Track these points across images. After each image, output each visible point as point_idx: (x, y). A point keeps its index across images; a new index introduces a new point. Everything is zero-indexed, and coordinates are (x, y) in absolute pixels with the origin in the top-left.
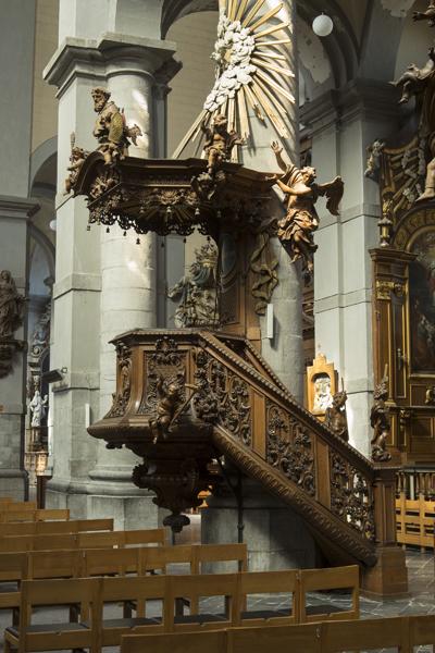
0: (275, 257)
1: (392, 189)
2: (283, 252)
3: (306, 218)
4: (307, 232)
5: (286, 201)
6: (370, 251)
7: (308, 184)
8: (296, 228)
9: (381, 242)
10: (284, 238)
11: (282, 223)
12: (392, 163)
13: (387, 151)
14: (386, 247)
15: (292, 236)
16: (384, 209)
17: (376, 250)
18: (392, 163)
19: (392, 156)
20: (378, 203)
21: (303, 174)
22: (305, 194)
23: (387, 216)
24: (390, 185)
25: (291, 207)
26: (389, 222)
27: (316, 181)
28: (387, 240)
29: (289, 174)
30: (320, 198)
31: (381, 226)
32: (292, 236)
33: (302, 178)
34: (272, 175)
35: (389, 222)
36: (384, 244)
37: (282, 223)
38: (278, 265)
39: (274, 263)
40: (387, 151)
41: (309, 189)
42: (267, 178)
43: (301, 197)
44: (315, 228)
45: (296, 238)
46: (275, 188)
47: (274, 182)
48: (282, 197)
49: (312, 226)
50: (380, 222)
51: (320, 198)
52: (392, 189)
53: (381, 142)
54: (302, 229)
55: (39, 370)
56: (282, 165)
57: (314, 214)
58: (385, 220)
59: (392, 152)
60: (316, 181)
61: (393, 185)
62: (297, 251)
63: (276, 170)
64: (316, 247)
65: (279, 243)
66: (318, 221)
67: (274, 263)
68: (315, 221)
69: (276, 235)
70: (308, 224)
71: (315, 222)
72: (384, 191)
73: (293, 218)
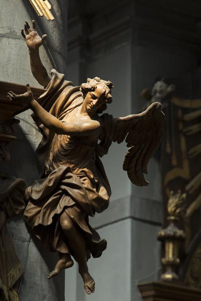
0: (17, 261)
1: (185, 172)
2: (33, 252)
3: (87, 184)
4: (86, 210)
5: (45, 148)
6: (141, 288)
7: (93, 113)
8: (65, 201)
9: (164, 270)
10: (38, 221)
11: (35, 191)
12: (187, 124)
13: (176, 101)
14: (173, 279)
15: (57, 218)
16: (170, 209)
17: (155, 285)
18: (187, 124)
19: (186, 111)
20: (157, 196)
21: (85, 91)
22: (89, 132)
23: (175, 222)
24: (180, 165)
25: (57, 159)
26: (180, 233)
27: (110, 110)
28: (174, 267)
29: (55, 93)
30: (114, 145)
31: (163, 240)
32: (57, 218)
33: (80, 100)
34: (23, 89)
35: (180, 233)
36: (168, 276)
37: (35, 191)
38: (21, 280)
39: (15, 274)
40: (176, 101)
41: (96, 123)
42: (11, 95)
43: (78, 137)
44: (102, 205)
45: (66, 223)
46: (25, 118)
47: (24, 104)
48: (36, 139)
49: (99, 199)
50: (162, 233)
51: (114, 145)
52: (185, 172)
53: (168, 82)
54: (78, 204)
55: (63, 187)
56: (39, 72)
57: (100, 178)
58: (171, 230)
59: (187, 104)
60: (110, 110)
61: (186, 164)
62: (64, 250)
63: (25, 78)
64: (103, 245)
65: (25, 233)
66: (109, 193)
67: (15, 274)
68: (102, 189)
69: (21, 216)
70: (91, 196)
71: (103, 193)
72: (171, 176)
73: (60, 181)
